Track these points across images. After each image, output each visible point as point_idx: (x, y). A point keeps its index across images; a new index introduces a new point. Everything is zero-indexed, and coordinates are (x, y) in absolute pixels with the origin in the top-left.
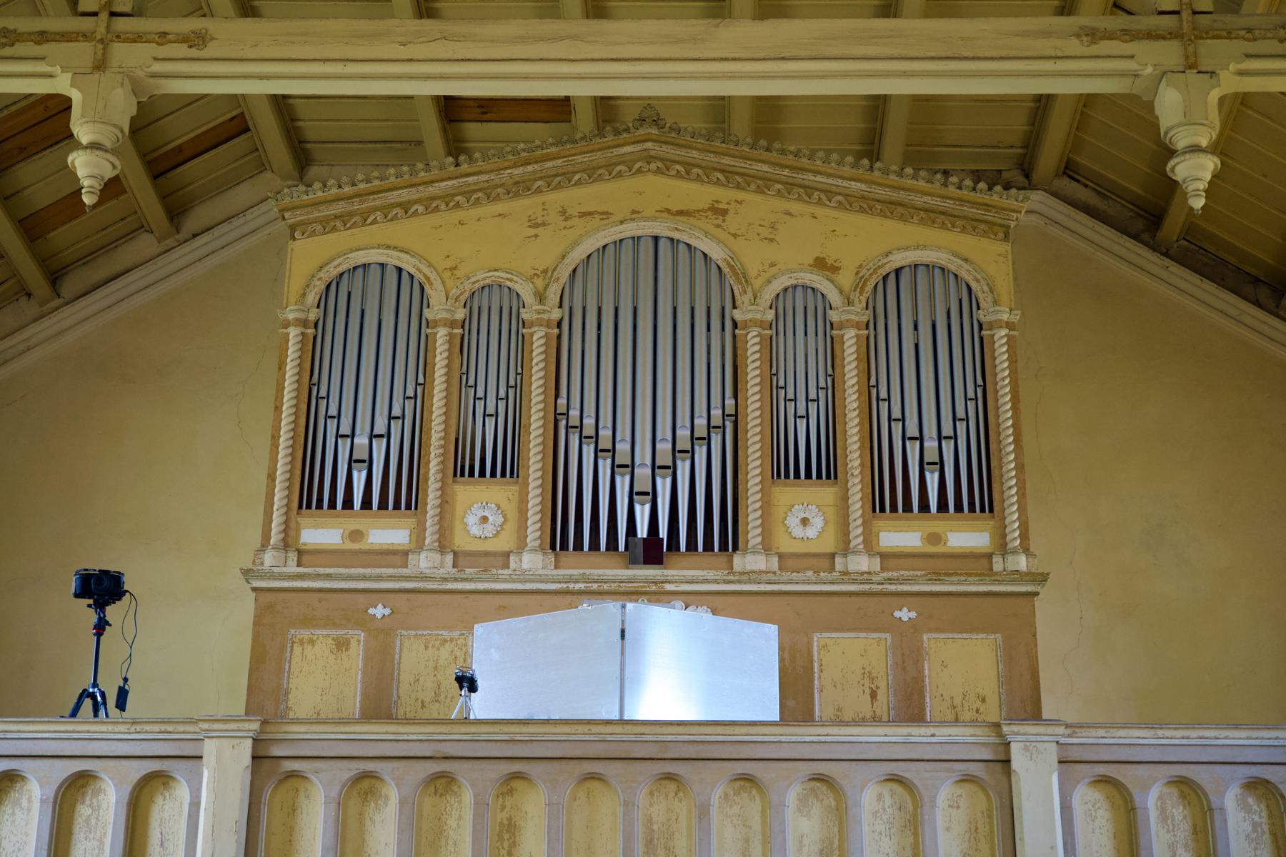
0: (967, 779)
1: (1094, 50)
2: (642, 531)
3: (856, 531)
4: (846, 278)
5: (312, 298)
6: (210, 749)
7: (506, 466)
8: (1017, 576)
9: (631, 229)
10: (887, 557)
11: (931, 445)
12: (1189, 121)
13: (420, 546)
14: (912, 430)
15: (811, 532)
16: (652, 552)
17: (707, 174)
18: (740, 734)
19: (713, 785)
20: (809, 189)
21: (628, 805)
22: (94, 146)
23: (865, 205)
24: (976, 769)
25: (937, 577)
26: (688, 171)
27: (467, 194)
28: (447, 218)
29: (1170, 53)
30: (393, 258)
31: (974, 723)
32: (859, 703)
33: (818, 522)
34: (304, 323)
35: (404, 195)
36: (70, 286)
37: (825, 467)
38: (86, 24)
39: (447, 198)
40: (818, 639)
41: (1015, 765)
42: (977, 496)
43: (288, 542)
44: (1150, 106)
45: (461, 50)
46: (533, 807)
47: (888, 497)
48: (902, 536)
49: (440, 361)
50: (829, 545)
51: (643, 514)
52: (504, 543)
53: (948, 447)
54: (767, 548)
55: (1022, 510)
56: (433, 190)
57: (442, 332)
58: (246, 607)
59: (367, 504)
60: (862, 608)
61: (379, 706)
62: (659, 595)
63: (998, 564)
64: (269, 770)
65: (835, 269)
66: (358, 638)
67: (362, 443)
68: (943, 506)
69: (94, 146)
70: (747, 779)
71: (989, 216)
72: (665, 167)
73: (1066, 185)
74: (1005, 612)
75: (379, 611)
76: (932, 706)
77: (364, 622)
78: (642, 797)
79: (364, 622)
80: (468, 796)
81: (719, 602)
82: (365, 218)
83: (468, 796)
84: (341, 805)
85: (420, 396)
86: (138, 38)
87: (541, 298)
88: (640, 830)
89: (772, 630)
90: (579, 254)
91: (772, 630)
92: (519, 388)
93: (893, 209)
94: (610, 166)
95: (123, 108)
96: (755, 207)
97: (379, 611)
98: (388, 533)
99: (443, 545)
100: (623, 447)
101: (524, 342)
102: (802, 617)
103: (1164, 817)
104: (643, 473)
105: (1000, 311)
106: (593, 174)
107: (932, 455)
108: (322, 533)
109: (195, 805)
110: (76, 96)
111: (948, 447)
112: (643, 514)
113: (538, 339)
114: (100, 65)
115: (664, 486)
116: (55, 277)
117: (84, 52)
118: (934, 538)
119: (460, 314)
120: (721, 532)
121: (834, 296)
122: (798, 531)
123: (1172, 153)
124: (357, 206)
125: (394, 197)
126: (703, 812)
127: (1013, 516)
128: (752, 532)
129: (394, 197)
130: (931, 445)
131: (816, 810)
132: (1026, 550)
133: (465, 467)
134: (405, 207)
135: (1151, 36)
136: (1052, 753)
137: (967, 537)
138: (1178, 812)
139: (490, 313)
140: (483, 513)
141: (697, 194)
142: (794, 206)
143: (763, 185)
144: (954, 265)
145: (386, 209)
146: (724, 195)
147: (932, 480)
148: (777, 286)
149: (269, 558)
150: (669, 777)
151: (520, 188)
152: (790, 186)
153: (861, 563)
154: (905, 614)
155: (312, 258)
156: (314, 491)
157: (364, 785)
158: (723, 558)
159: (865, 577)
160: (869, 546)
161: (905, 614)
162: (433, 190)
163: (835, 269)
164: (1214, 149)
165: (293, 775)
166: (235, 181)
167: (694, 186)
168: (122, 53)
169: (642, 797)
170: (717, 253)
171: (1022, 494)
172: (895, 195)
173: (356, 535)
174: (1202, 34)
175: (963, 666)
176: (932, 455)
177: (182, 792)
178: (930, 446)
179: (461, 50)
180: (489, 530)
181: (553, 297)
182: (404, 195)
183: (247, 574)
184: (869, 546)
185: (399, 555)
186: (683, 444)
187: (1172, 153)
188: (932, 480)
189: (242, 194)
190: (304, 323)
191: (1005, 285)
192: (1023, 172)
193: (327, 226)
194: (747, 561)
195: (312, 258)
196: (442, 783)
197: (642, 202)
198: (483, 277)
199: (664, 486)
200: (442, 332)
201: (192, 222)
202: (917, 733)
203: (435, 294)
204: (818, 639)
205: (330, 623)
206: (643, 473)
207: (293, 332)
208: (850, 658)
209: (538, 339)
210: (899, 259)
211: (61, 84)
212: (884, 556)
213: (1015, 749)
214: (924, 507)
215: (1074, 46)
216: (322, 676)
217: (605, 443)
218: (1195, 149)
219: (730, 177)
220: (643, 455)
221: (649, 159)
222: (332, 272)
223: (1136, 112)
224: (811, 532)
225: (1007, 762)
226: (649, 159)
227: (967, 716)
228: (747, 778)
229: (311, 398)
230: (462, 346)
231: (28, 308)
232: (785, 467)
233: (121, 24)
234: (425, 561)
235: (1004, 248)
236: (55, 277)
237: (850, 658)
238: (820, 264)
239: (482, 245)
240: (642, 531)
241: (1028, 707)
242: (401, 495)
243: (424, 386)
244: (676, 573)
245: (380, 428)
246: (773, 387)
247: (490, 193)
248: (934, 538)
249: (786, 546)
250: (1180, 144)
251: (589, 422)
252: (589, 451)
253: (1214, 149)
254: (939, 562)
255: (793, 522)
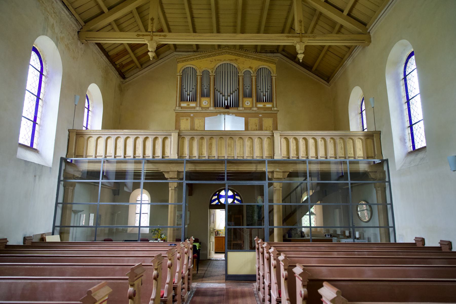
0: (268, 138)
1: (288, 39)
2: (226, 105)
3: (254, 105)
4: (254, 69)
5: (181, 72)
6: (172, 134)
7: (208, 96)
8: (275, 110)
9: (224, 62)
10: (258, 108)
11: (264, 93)
12: (300, 50)
13: (197, 106)
14: (262, 91)
15: (248, 105)
16: (227, 107)
17: (235, 54)
18: (240, 132)
19: (237, 139)
20: (249, 57)
21: (226, 141)
22: (152, 51)
23: (256, 59)
24: (269, 136)
25: (265, 111)
26: (232, 54)
27: (202, 57)
28: (199, 60)
29: (298, 39)
30: (192, 66)
31: (269, 131)
32: (254, 127)
33: (249, 103)
34: (180, 75)
35: (193, 57)
36: (144, 66)
37: (250, 96)
38: (149, 33)
39: (199, 57)
40: (249, 119)
41: (274, 136)
42: (270, 100)
43: (180, 106)
44: (295, 47)
45: (202, 38)
46: (214, 141)
47: (259, 100)
48: (260, 105)
49: (199, 81)
50: (251, 106)
51: (226, 102)
52: (208, 106)
53: (266, 93)
54: (243, 107)
55: (276, 101)
56: (197, 56)
57: (199, 77)
58: (174, 115)
59: (190, 101)
60: (255, 115)
61: (192, 129)
62: (228, 113)
63: (273, 109)
64: (181, 137)
65: (252, 68)
66: (189, 118)
67: (189, 93)
68: (266, 101)
69: (152, 51)
70: (241, 138)
71: (273, 61)
72: (229, 53)
73: (283, 53)
74: (274, 116)
75: (192, 115)
76: (264, 128)
77: (190, 116)
78: (227, 140)
79: (190, 116)
80: (205, 140)
81: (238, 115)
82: (188, 60)
83: (205, 140)
84: (190, 141)
85: (196, 85)
86: (157, 36)
87: (212, 72)
88: (227, 144)
89: (244, 118)
90: (217, 66)
91: (244, 118)
92: (210, 84)
93: (260, 60)
94: (221, 53)
95: (155, 46)
96: (241, 59)
97: (192, 115)
98: (193, 105)
99: (200, 106)
100: (223, 93)
101: (210, 78)
102: (247, 116)
103: (292, 142)
104: (226, 96)
105: (274, 74)
106: (219, 54)
107: (264, 94)
108: (184, 105)
109: (171, 141)
110: (148, 44)
111: (266, 93)
112: (226, 102)
113: (212, 78)
114: (152, 40)
115: (229, 98)
116: (141, 65)
117: (149, 38)
118: (264, 105)
119: (201, 74)
120: (236, 105)
121: (252, 72)
122: (247, 104)
123: (298, 54)
124: (187, 59)
125: (192, 57)
126: (235, 142)
127: (275, 103)
128: (241, 105)
129: (192, 57)
130: (264, 93)
131: (249, 142)
132: (276, 107)
133: (203, 95)
134: (193, 59)
135: (296, 37)
136: (279, 134)
137: (269, 105)
138: (294, 142)
139: (205, 73)
140: (205, 102)
141: (233, 57)
142: (247, 59)
143: (242, 56)
144: (268, 68)
145: (191, 59)
146: (237, 57)
147: (264, 98)
148: (244, 71)
149: (177, 108)
150: (231, 137)
151: (209, 56)
152: (246, 56)
153: (255, 109)
154: (260, 116)
155: (181, 66)
156: (182, 99)
157: (192, 139)
158: (237, 108)
159: (255, 111)
160: (256, 106)
161: (260, 116)
162: (197, 56)
163: (252, 68)
164: (303, 53)
165: (183, 137)
166: (166, 51)
167: (233, 56)
168: (155, 38)
169: (227, 140)
170: (236, 66)
171: (276, 99)
172: (260, 58)
173: (188, 105)
174: (303, 37)
175: (268, 122)
176: (264, 94)
177: (169, 139)
178: (264, 94)
179: (202, 38)
180: (206, 104)
181: (214, 72)
182: (193, 57)
183: (174, 110)
184: (256, 106)
185: (194, 108)
186: (232, 92)
187: (298, 54)
188: (264, 98)
189: (167, 53)
190: (180, 75)
191: (275, 70)
192: (278, 52)
193: (183, 61)
194: (240, 108)
195: (181, 66)
196: (202, 138)
197: (226, 58)
198: (204, 69)
199: (229, 98)
200: (199, 77)
201: (160, 57)
202: (262, 132)
203: (198, 71)
204: (249, 119)
205: (185, 117)
206: (226, 96)
207: (179, 77)
208: (253, 121)
209: (212, 78)
210: (261, 67)
211: (146, 42)
212: (258, 108)
213: (274, 134)
214: (263, 101)
215: (285, 38)
216: (185, 124)
217: (223, 94)
218: (301, 53)
219: (238, 55)
220: (226, 94)
221: (227, 52)
222: (183, 68)
223: (294, 47)
224: (248, 105)
225: (273, 135)
226: (227, 52)
227: (268, 129)
228: (241, 138)
229: (181, 86)
230: (201, 79)
231: (138, 70)
232: (245, 96)
233: (154, 33)
234: (198, 108)
235: (275, 65)
236: (141, 65)
237: (253, 121)
238: (250, 68)
239: (203, 64)
240: (226, 105)
241: (276, 129)
242: (194, 99)
243: (197, 84)
244: (230, 110)
245: (191, 90)
246: (243, 85)
247: (205, 57)
248: (264, 105)
249: (245, 106)
250: (299, 52)
251: (219, 89)
252: (219, 93)
253: (303, 53)
254: (265, 109)
255: (246, 103)
